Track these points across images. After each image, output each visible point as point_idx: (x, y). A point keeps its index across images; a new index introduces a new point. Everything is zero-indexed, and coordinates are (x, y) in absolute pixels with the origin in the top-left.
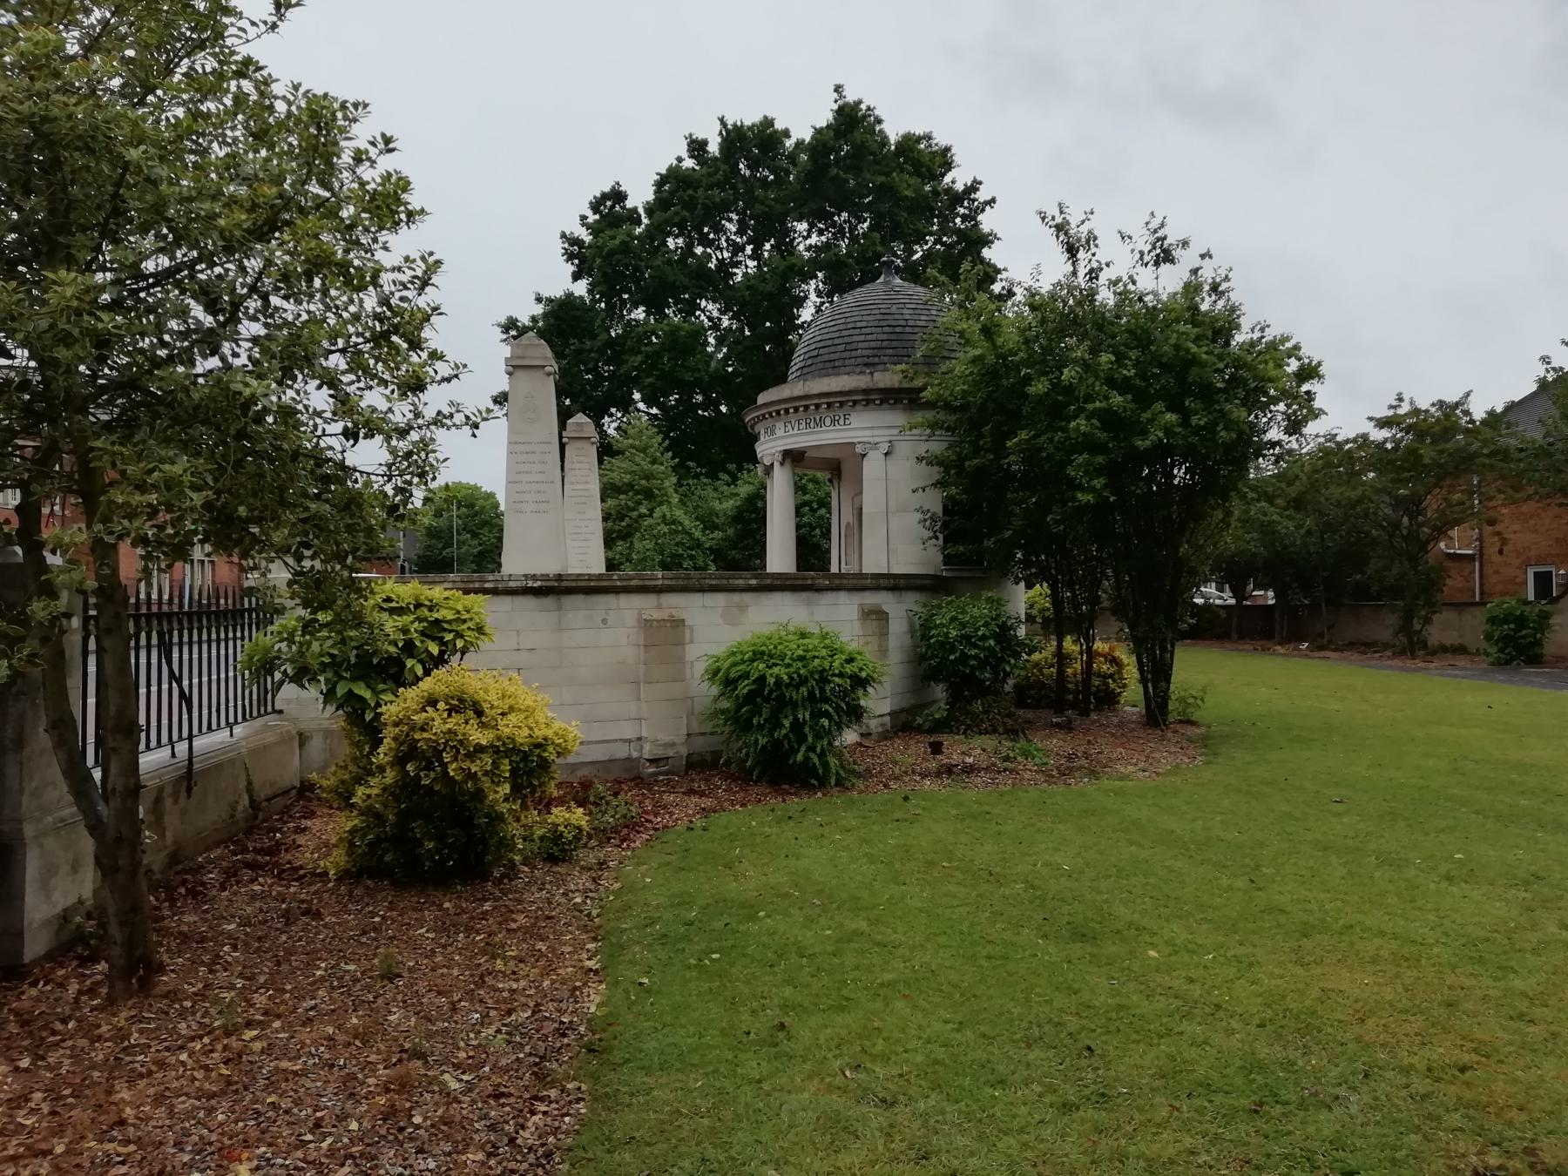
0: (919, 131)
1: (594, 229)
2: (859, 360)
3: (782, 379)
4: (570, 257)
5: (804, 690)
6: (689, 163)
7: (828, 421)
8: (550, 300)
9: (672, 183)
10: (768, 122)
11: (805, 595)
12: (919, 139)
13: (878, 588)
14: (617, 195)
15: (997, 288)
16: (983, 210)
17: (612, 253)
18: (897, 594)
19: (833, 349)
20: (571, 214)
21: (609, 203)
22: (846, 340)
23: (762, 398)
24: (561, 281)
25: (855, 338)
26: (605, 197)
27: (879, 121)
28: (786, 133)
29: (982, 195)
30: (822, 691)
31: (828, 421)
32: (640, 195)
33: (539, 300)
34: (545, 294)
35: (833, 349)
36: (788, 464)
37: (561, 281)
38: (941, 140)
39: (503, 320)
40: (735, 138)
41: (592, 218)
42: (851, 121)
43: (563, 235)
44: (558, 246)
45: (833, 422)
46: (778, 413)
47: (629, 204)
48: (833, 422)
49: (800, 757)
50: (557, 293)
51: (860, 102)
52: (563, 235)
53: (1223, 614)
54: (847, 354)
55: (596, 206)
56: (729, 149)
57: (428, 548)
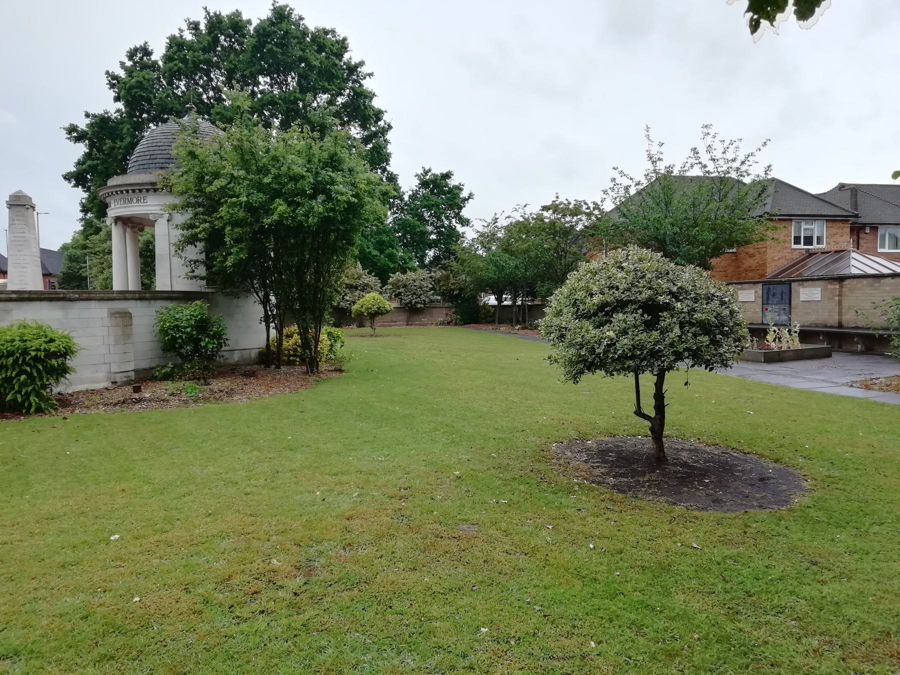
0: (328, 27)
1: (130, 72)
2: (158, 165)
3: (124, 171)
4: (112, 86)
5: (11, 360)
6: (188, 36)
7: (135, 200)
8: (94, 116)
9: (176, 45)
10: (238, 14)
11: (60, 303)
12: (326, 32)
13: (125, 299)
14: (146, 52)
15: (381, 123)
16: (365, 78)
17: (131, 88)
18: (146, 303)
19: (143, 158)
20: (116, 61)
21: (139, 55)
22: (151, 153)
23: (111, 182)
24: (108, 104)
25: (156, 152)
26: (136, 50)
27: (301, 19)
28: (249, 22)
29: (364, 70)
30: (24, 359)
31: (135, 200)
32: (158, 54)
33: (87, 115)
34: (91, 112)
35: (143, 158)
36: (119, 223)
37: (108, 104)
38: (341, 33)
39: (67, 125)
40: (216, 23)
41: (129, 64)
42: (281, 15)
43: (107, 73)
44: (105, 80)
45: (138, 201)
46: (122, 192)
47: (153, 58)
48: (138, 201)
49: (9, 397)
50: (99, 111)
51: (287, 6)
52: (107, 73)
53: (492, 310)
54: (151, 161)
55: (131, 55)
56: (210, 27)
57: (69, 268)
